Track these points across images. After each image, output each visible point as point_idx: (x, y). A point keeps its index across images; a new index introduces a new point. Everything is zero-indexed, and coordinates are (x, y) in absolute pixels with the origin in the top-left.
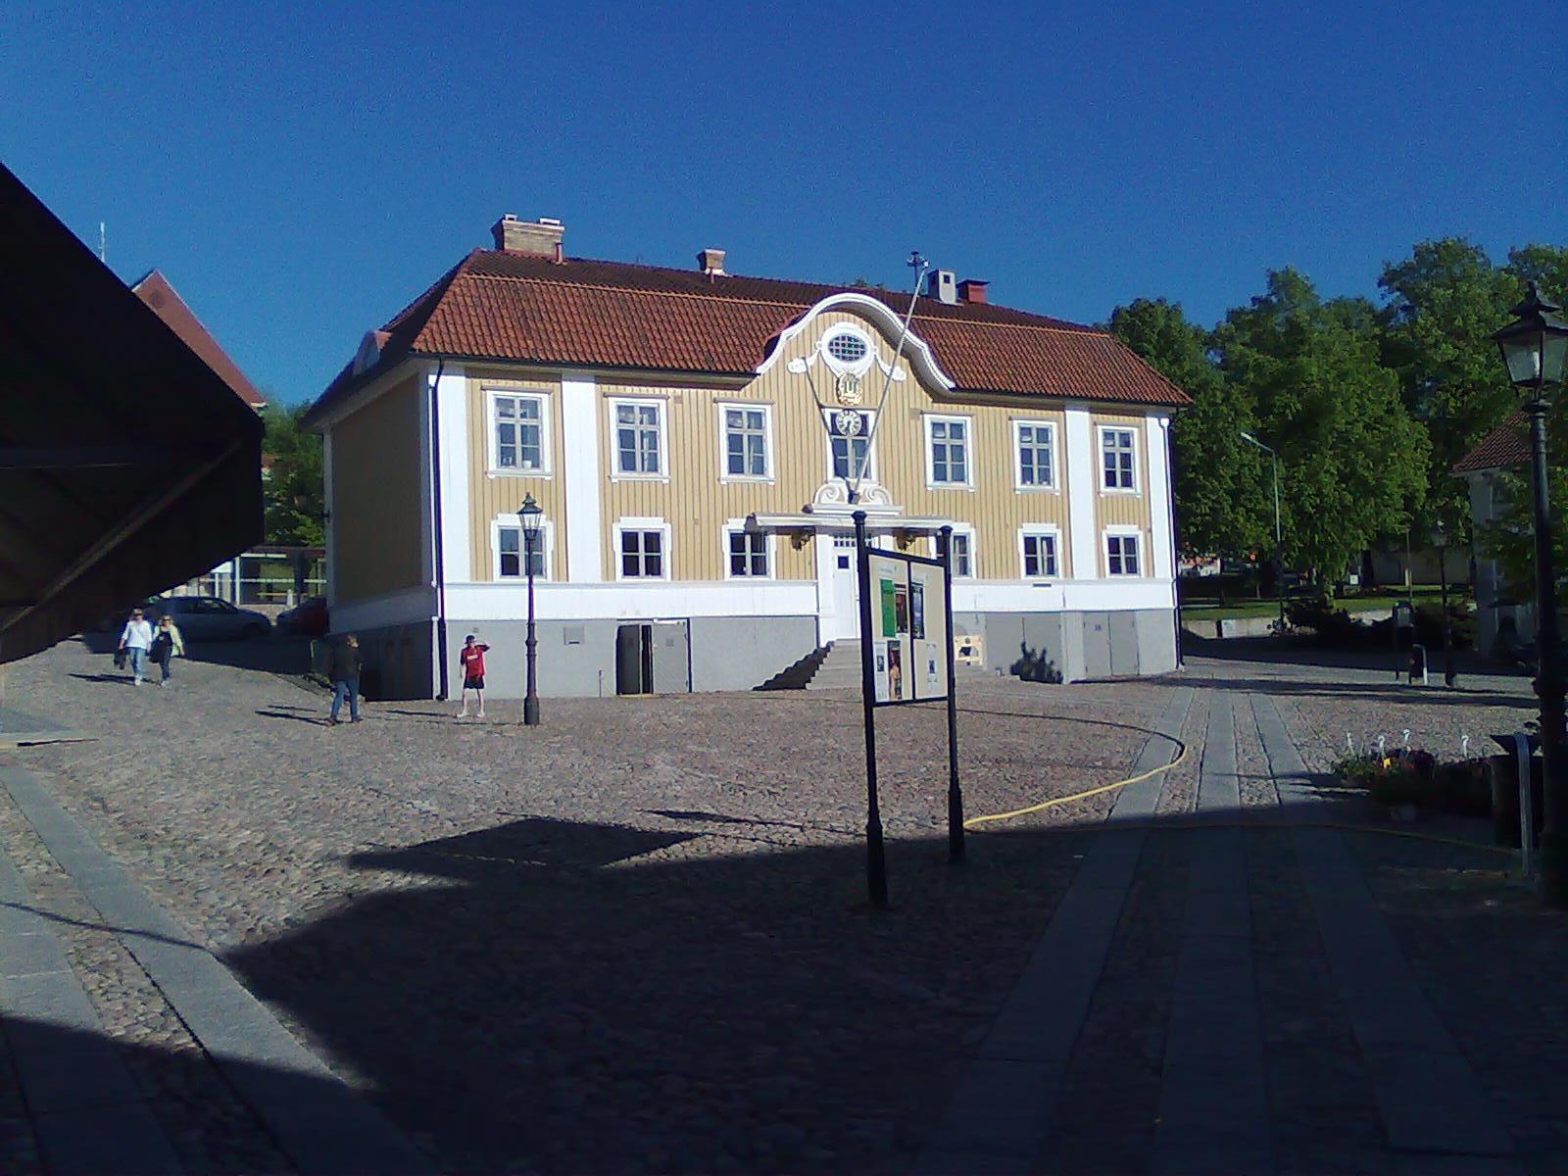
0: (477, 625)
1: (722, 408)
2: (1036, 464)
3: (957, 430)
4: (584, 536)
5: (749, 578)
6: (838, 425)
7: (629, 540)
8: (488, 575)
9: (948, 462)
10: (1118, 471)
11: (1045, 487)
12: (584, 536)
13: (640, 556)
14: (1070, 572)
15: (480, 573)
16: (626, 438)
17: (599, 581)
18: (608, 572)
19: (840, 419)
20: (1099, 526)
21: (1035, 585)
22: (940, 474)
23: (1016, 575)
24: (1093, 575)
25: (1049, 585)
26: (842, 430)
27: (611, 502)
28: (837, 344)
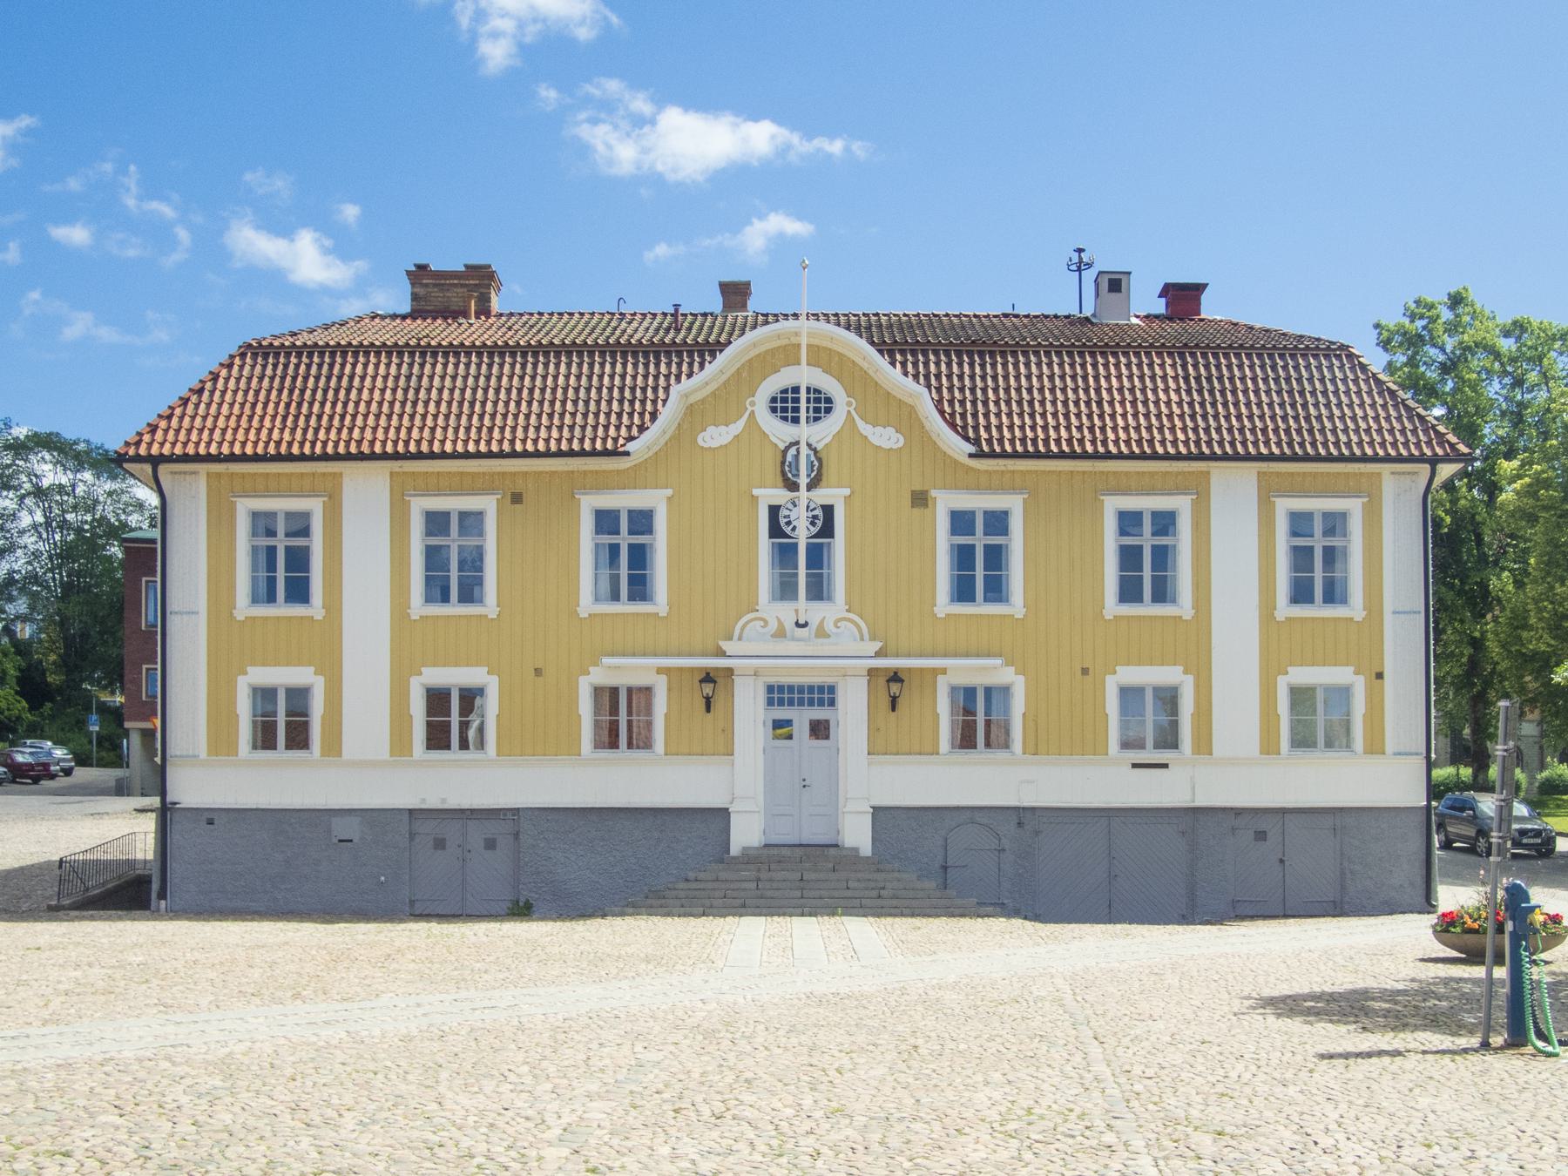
0: (215, 816)
1: (245, 507)
2: (1146, 569)
3: (998, 522)
4: (367, 699)
5: (281, 754)
6: (782, 521)
7: (437, 699)
8: (232, 749)
9: (979, 569)
10: (1315, 571)
11: (298, 610)
12: (367, 699)
13: (448, 720)
14: (1204, 744)
15: (222, 742)
16: (1302, 557)
17: (385, 754)
18: (400, 744)
19: (787, 512)
20: (1269, 673)
21: (1135, 766)
22: (1129, 592)
23: (1100, 749)
24: (1253, 745)
25: (1165, 766)
26: (788, 530)
27: (1277, 647)
28: (784, 400)
